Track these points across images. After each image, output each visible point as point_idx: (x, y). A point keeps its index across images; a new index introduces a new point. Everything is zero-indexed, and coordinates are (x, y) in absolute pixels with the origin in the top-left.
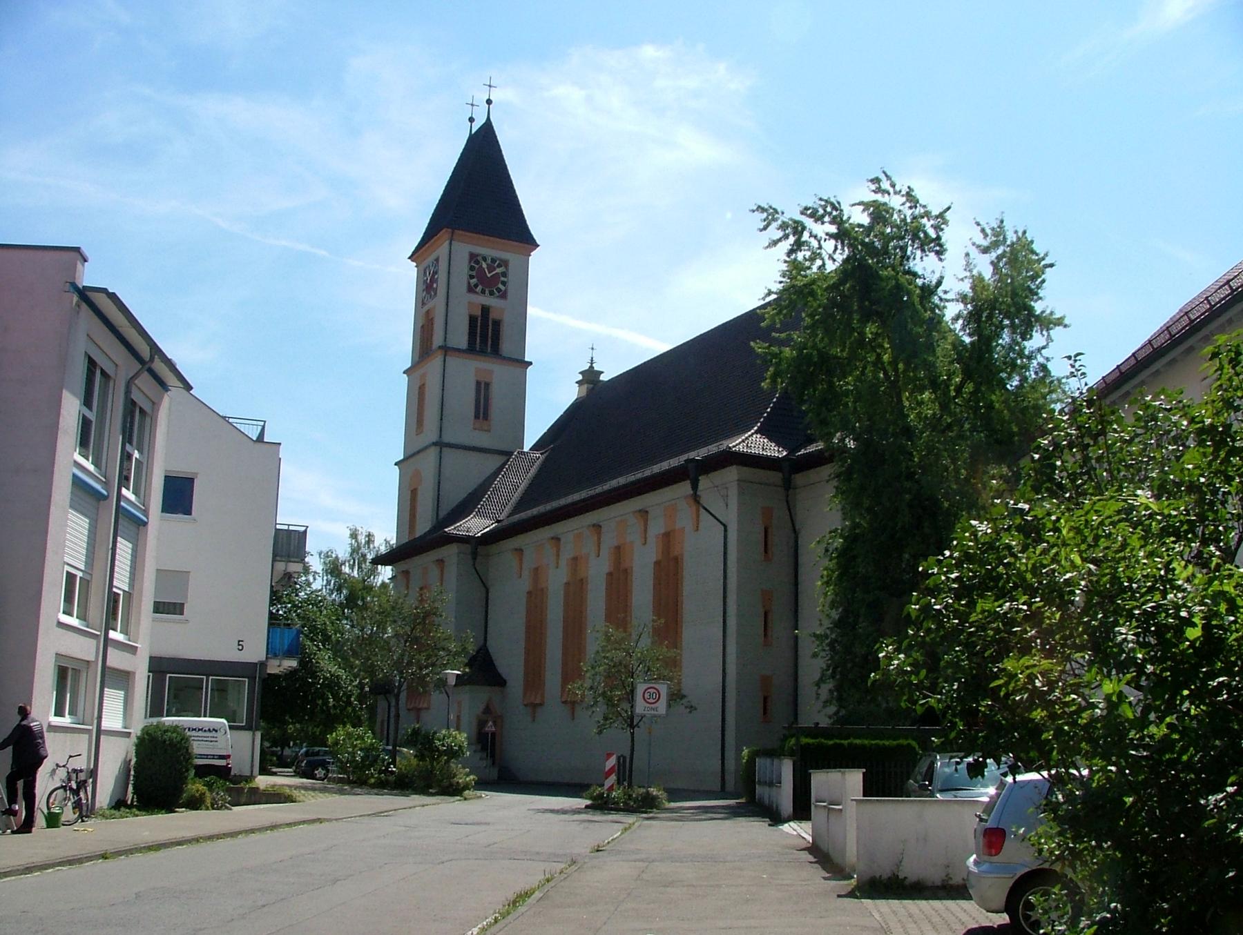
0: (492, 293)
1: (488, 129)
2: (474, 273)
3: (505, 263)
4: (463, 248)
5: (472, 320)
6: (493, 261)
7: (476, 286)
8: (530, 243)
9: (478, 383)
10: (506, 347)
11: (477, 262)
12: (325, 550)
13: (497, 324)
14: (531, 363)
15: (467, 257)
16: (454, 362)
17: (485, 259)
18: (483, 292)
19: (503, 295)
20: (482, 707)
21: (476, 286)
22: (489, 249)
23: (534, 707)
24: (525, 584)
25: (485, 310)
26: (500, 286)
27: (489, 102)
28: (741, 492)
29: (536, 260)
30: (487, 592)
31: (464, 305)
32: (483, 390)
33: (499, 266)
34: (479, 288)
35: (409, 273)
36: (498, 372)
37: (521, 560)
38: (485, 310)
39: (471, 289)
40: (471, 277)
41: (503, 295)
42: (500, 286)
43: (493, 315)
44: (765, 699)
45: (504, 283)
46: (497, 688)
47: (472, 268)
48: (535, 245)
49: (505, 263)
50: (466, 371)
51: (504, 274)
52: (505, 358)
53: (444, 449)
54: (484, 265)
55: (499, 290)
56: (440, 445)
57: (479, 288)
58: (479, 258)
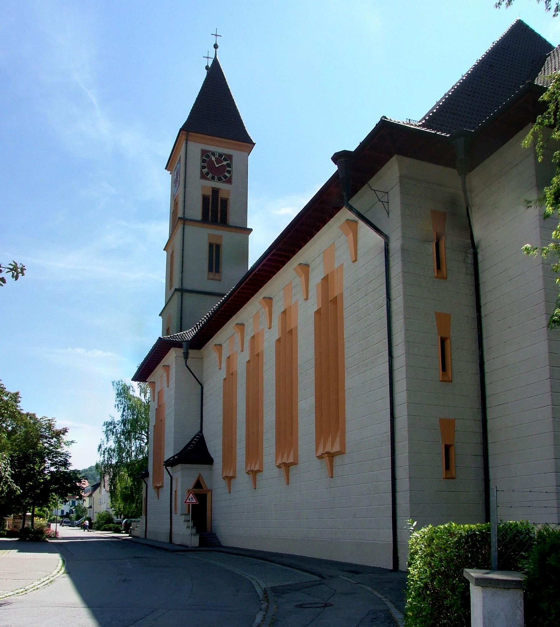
0: (220, 179)
1: (216, 62)
2: (205, 165)
3: (229, 157)
4: (195, 148)
5: (205, 199)
6: (220, 155)
7: (207, 174)
8: (246, 143)
9: (211, 245)
10: (232, 219)
11: (208, 156)
12: (117, 381)
13: (225, 202)
14: (251, 230)
15: (199, 153)
16: (190, 229)
17: (213, 154)
18: (213, 178)
19: (229, 181)
20: (193, 482)
21: (207, 174)
22: (218, 148)
23: (229, 479)
24: (223, 374)
25: (215, 191)
26: (226, 174)
27: (216, 46)
28: (404, 193)
29: (254, 158)
30: (202, 388)
31: (199, 187)
32: (215, 250)
33: (225, 160)
34: (210, 176)
35: (167, 177)
36: (226, 237)
37: (220, 353)
38: (215, 191)
39: (203, 176)
40: (203, 167)
41: (229, 181)
42: (226, 174)
43: (222, 195)
44: (447, 448)
45: (229, 172)
46: (207, 466)
47: (204, 161)
48: (254, 144)
49: (229, 157)
50: (200, 237)
51: (229, 165)
52: (231, 227)
53: (186, 295)
54: (213, 159)
55: (225, 177)
56: (182, 291)
57: (210, 176)
58: (210, 154)
